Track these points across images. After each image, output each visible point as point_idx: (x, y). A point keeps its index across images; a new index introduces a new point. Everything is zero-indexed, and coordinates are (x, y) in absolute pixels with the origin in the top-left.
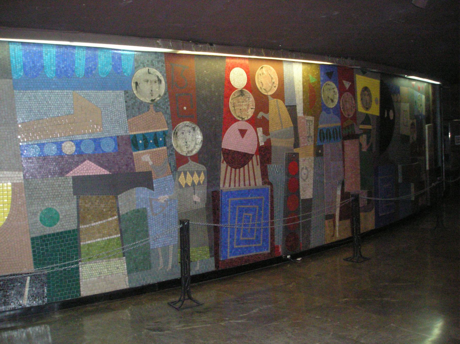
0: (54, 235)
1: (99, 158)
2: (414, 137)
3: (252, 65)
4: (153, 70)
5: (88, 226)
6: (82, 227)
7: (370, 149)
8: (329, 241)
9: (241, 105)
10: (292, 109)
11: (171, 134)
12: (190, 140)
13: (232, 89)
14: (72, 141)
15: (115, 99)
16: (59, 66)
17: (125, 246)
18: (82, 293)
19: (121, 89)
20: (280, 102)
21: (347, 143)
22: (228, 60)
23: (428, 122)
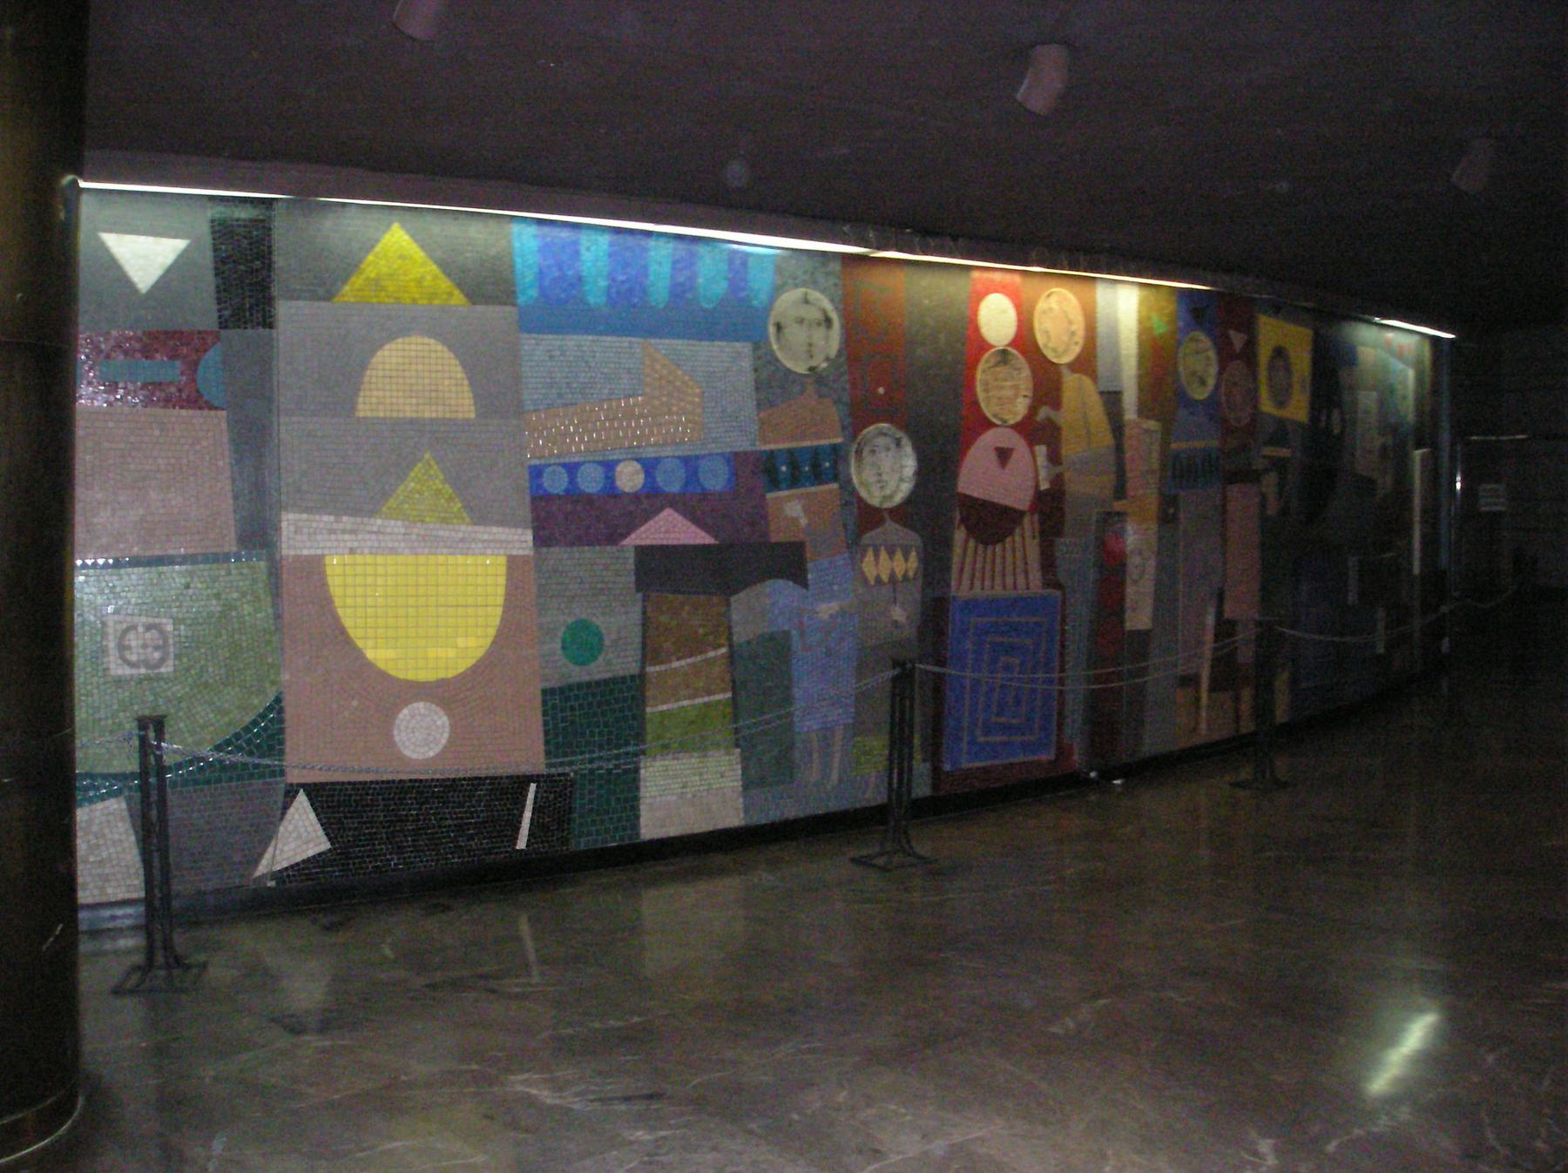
0: (589, 685)
1: (693, 505)
2: (1386, 483)
3: (1028, 288)
4: (815, 295)
5: (663, 667)
6: (650, 669)
7: (1284, 512)
8: (1184, 743)
9: (1002, 388)
10: (1112, 399)
11: (847, 453)
12: (889, 472)
13: (984, 346)
14: (637, 460)
15: (729, 360)
16: (614, 280)
17: (741, 723)
18: (643, 831)
19: (747, 338)
20: (1087, 381)
21: (1234, 490)
22: (976, 274)
23: (1418, 445)
